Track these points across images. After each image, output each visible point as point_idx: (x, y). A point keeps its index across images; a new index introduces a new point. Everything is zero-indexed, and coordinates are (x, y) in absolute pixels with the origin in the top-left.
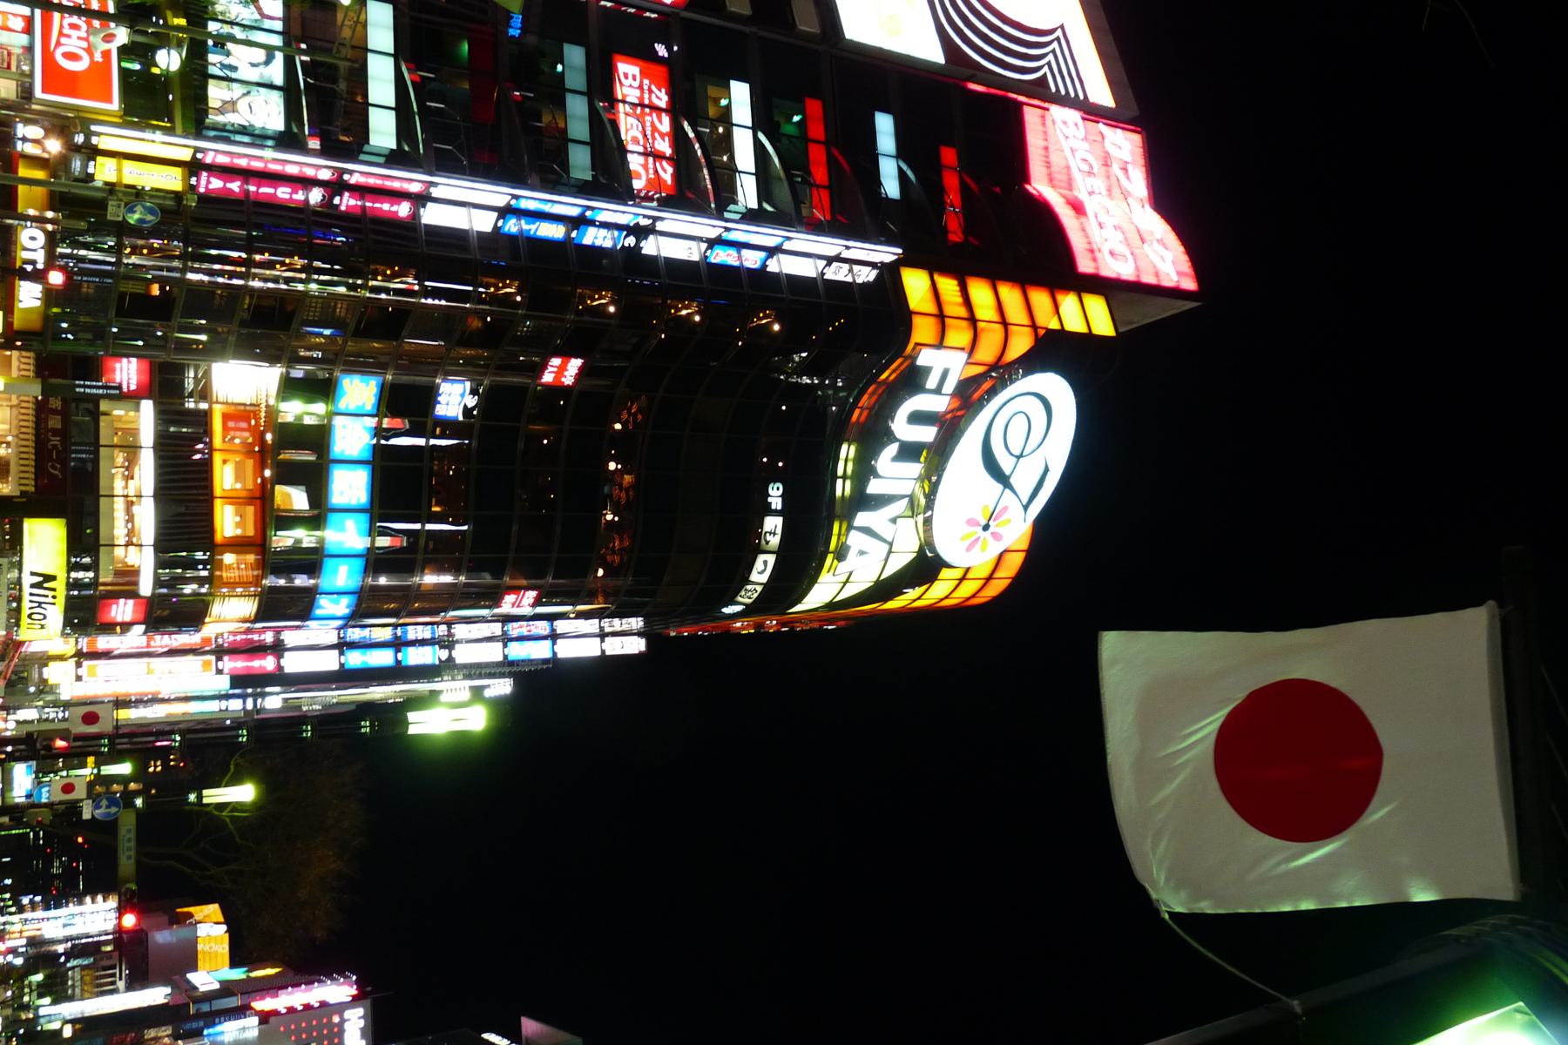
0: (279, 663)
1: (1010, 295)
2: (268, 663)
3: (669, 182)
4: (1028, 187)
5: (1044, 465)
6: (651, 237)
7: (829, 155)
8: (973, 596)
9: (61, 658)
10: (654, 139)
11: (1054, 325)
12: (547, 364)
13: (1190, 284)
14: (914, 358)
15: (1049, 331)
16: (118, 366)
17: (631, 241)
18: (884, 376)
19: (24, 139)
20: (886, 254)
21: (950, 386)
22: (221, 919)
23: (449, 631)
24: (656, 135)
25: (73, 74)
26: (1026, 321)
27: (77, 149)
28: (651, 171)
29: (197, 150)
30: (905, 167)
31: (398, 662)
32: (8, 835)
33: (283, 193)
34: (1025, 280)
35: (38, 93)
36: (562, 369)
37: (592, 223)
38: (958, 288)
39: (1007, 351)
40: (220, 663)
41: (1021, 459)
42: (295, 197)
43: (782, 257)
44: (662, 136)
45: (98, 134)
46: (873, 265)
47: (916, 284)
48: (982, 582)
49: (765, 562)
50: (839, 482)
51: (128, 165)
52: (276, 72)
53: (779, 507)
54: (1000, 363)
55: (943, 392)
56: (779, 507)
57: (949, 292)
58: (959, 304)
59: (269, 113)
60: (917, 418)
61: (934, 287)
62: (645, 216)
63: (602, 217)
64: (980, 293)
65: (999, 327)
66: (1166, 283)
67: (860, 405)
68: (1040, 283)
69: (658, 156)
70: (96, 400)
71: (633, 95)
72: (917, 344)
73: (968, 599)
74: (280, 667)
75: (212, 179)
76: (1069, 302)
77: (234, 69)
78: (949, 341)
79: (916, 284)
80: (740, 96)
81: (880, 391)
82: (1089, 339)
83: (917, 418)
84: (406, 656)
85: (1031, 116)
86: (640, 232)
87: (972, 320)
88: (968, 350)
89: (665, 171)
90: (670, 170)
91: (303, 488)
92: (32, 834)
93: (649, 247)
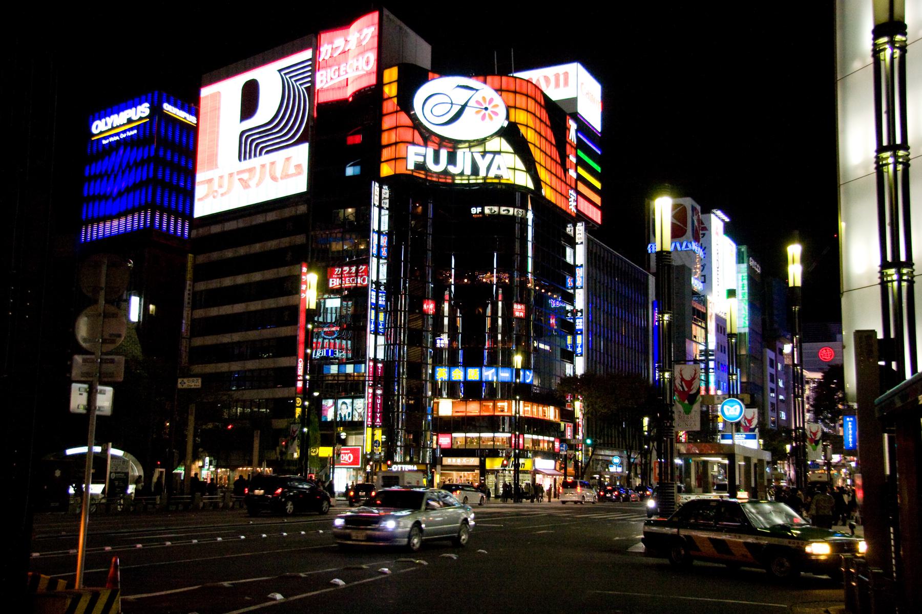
1: (387, 123)
11: (395, 100)
13: (375, 16)
15: (398, 104)
17: (382, 288)
20: (375, 187)
21: (421, 150)
23: (570, 312)
25: (354, 457)
29: (367, 426)
33: (379, 401)
34: (379, 115)
35: (360, 466)
39: (407, 125)
47: (386, 170)
49: (504, 211)
52: (348, 401)
53: (480, 208)
56: (480, 208)
57: (389, 154)
59: (360, 403)
60: (437, 161)
61: (386, 161)
63: (374, 301)
66: (376, 33)
69: (357, 271)
76: (386, 90)
77: (349, 413)
78: (403, 154)
79: (386, 170)
83: (437, 161)
85: (323, 98)
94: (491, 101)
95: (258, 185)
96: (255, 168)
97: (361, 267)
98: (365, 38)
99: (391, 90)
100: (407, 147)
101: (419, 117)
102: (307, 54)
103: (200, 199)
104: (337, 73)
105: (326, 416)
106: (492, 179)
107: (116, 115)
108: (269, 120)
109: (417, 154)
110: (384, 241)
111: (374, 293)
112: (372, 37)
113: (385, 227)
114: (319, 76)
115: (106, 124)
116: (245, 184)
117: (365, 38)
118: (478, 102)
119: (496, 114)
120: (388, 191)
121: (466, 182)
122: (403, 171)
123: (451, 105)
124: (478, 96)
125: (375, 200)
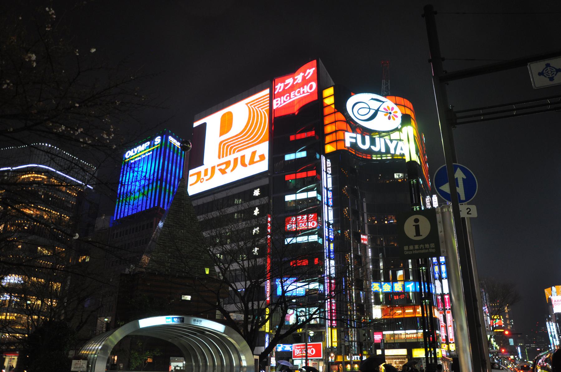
0: (446, 294)
1: (327, 120)
2: (447, 297)
3: (313, 215)
4: (296, 113)
5: (371, 100)
6: (329, 222)
7: (299, 172)
8: (410, 109)
9: (449, 347)
10: (303, 220)
11: (333, 106)
12: (363, 243)
13: (315, 62)
14: (348, 147)
15: (335, 108)
16: (376, 339)
17: (331, 226)
18: (354, 153)
19: (332, 360)
20: (323, 159)
21: (354, 135)
22: (550, 288)
24: (303, 219)
26: (334, 115)
27: (332, 350)
28: (312, 220)
29: (328, 327)
30: (298, 151)
31: (444, 264)
32: (528, 355)
34: (322, 116)
35: (322, 358)
36: (363, 239)
37: (329, 236)
38: (328, 136)
40: (448, 309)
41: (370, 108)
42: (334, 305)
43: (328, 187)
44: (302, 218)
45: (329, 346)
46: (326, 161)
47: (329, 149)
48: (406, 108)
50: (383, 158)
51: (333, 340)
54: (346, 121)
55: (355, 137)
58: (332, 136)
60: (364, 142)
61: (328, 143)
62: (325, 225)
63: (327, 235)
64: (329, 129)
65: (337, 123)
67: (362, 157)
68: (322, 111)
69: (308, 218)
70: (384, 343)
71: (294, 226)
72: (345, 147)
73: (411, 110)
74: (448, 294)
75: (333, 323)
78: (342, 138)
79: (329, 149)
80: (289, 198)
81: (358, 152)
82: (335, 95)
83: (364, 142)
84: (442, 262)
86: (329, 224)
87: (336, 131)
88: (344, 132)
89: (311, 216)
90: (310, 215)
91: (397, 272)
92: (527, 348)
93: (332, 222)
94: (393, 109)
95: (232, 171)
96: (230, 161)
97: (310, 215)
98: (308, 75)
99: (329, 101)
100: (344, 133)
101: (350, 114)
102: (267, 91)
103: (191, 185)
104: (288, 98)
105: (288, 321)
106: (397, 156)
107: (140, 146)
108: (239, 132)
109: (351, 137)
110: (330, 195)
111: (327, 230)
112: (313, 74)
113: (330, 186)
114: (275, 102)
115: (134, 152)
116: (223, 172)
117: (308, 75)
118: (385, 109)
119: (396, 116)
120: (330, 163)
121: (380, 158)
122: (343, 148)
123: (369, 110)
124: (384, 106)
125: (324, 167)
